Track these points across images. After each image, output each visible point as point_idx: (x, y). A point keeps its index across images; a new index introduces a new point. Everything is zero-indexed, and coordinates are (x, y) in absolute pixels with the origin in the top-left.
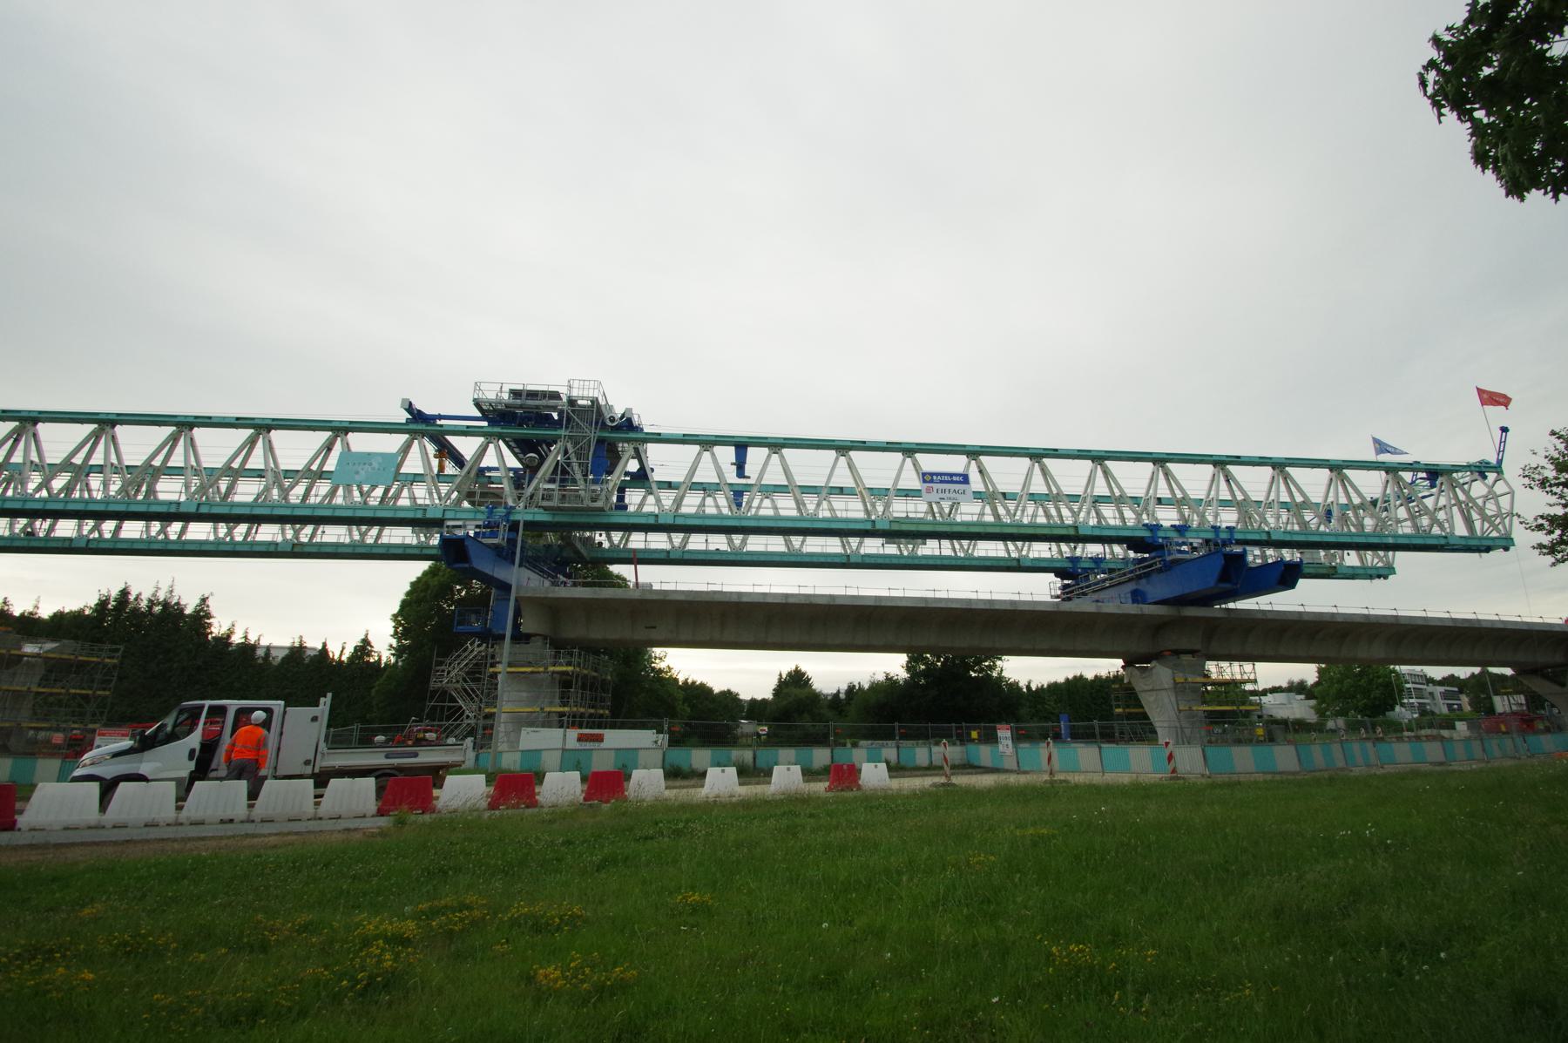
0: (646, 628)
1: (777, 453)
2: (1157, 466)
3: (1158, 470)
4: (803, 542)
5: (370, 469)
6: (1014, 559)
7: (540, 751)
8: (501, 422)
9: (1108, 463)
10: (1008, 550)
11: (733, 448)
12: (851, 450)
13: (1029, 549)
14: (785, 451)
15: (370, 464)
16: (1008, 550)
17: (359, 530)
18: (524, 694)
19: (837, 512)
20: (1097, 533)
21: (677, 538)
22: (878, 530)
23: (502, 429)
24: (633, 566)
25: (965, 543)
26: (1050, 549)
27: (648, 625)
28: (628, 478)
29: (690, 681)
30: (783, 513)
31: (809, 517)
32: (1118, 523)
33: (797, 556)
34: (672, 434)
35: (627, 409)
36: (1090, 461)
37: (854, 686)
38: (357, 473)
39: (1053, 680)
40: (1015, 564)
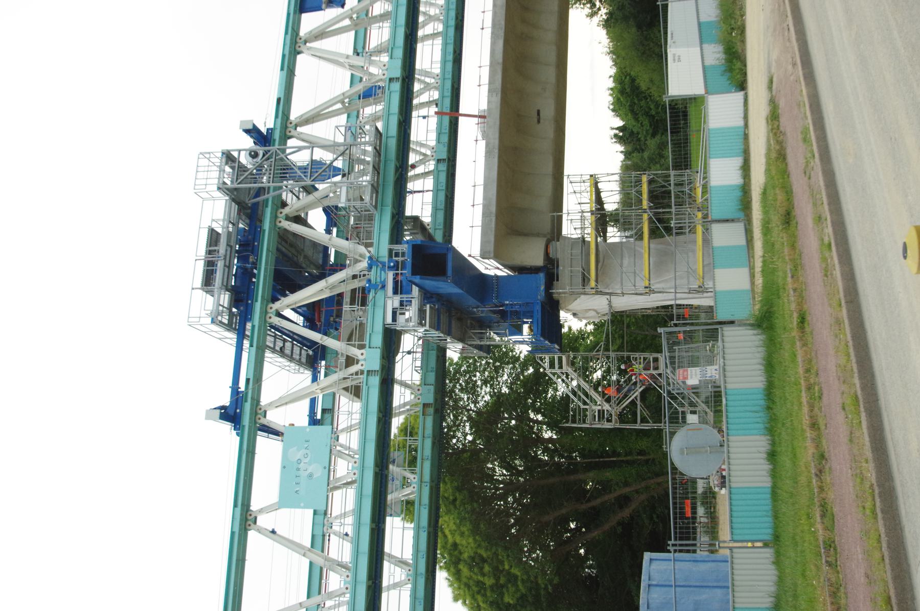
0: (539, 122)
1: (265, 412)
2: (303, 48)
3: (311, 48)
4: (404, 384)
5: (307, 460)
6: (437, 166)
7: (700, 24)
8: (247, 304)
9: (294, 115)
10: (433, 36)
11: (304, 16)
12: (258, 401)
13: (422, 145)
14: (255, 506)
15: (299, 461)
16: (433, 36)
17: (421, 92)
18: (626, 262)
19: (354, 422)
20: (399, 53)
21: (391, 573)
22: (383, 367)
23: (256, 301)
24: (461, 119)
25: (413, 158)
26: (424, 117)
27: (536, 120)
28: (335, 230)
29: (612, 107)
30: (351, 505)
31: (356, 472)
32: (388, 25)
33: (448, 10)
34: (280, 85)
35: (240, 128)
36: (299, 57)
37: (616, 136)
38: (311, 476)
39: (606, 99)
40: (443, 167)
